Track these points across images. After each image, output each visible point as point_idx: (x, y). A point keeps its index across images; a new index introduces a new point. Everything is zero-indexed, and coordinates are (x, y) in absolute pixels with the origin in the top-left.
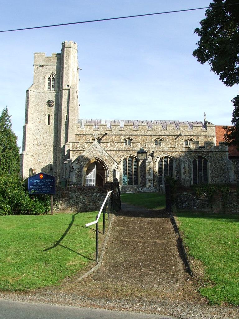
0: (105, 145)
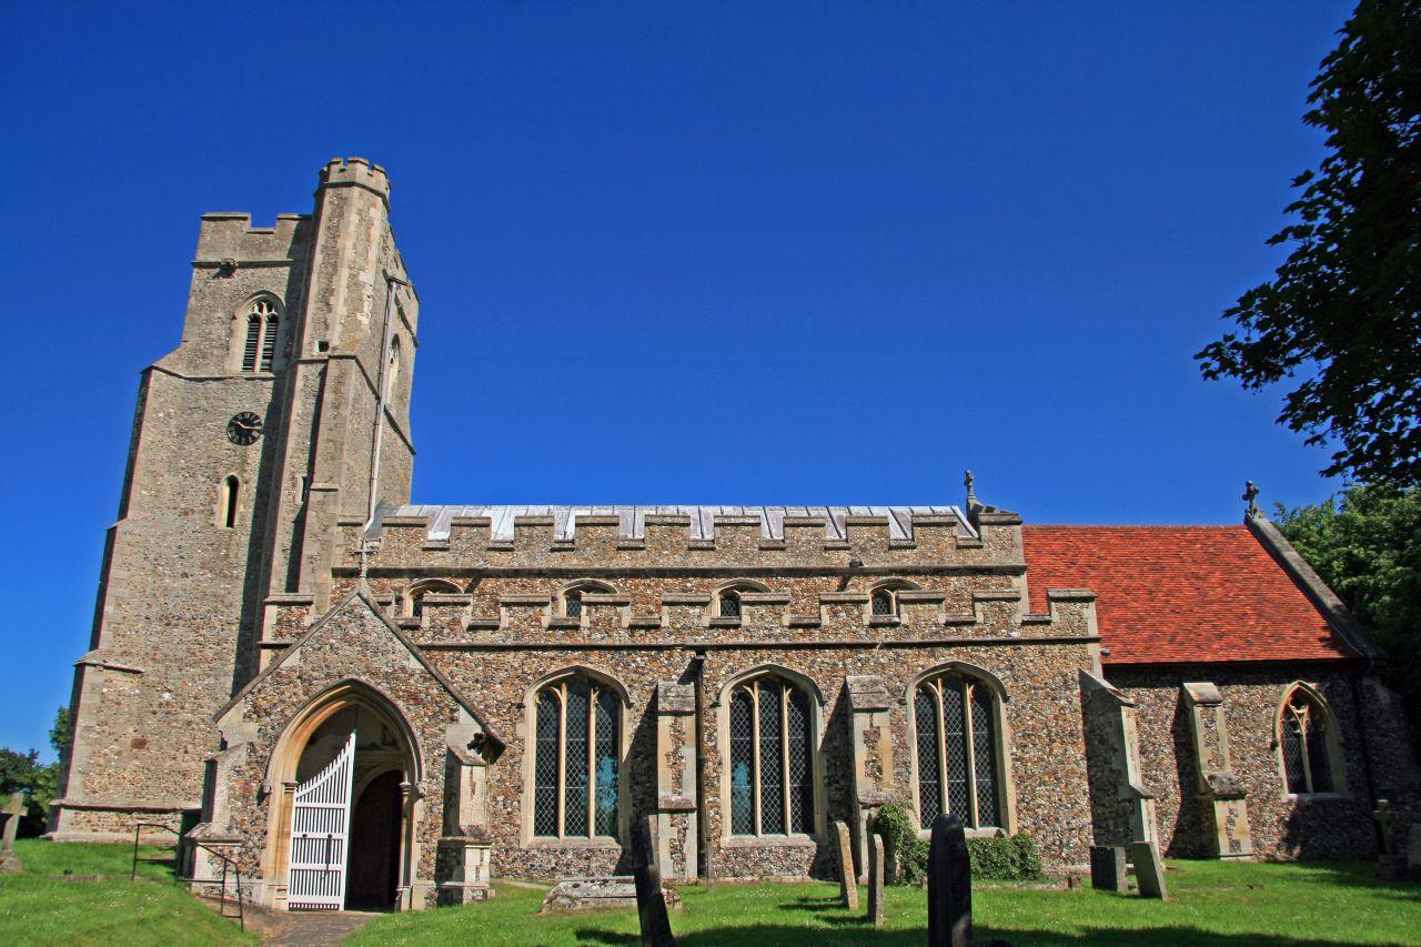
0: (442, 613)
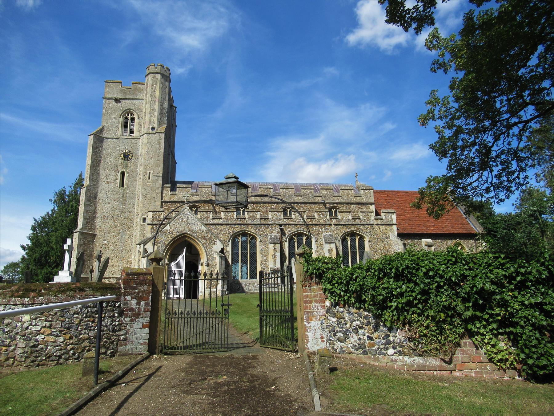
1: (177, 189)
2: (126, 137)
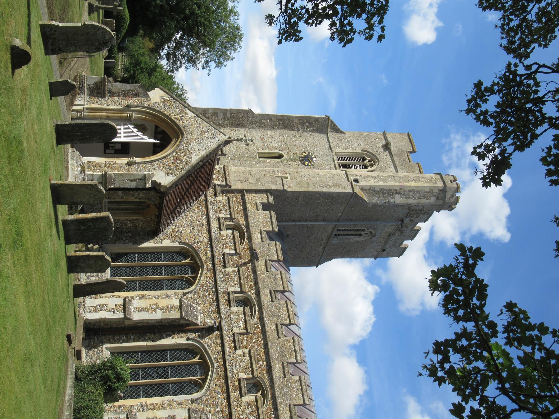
0: (224, 206)
1: (268, 212)
2: (335, 158)
